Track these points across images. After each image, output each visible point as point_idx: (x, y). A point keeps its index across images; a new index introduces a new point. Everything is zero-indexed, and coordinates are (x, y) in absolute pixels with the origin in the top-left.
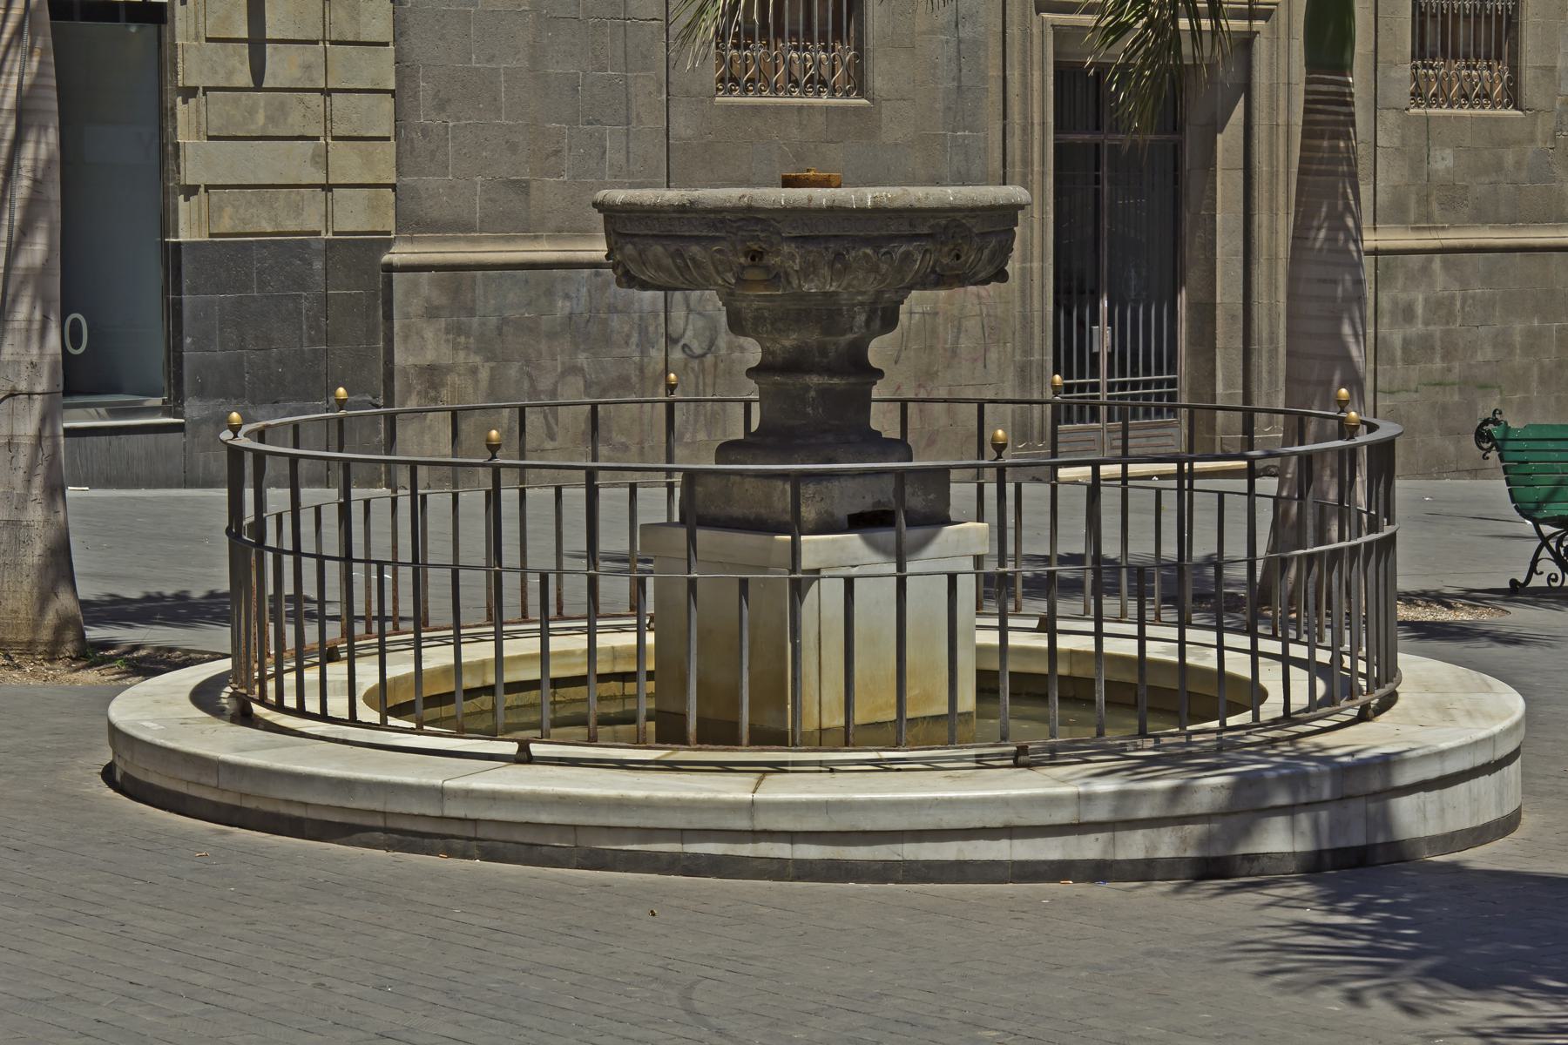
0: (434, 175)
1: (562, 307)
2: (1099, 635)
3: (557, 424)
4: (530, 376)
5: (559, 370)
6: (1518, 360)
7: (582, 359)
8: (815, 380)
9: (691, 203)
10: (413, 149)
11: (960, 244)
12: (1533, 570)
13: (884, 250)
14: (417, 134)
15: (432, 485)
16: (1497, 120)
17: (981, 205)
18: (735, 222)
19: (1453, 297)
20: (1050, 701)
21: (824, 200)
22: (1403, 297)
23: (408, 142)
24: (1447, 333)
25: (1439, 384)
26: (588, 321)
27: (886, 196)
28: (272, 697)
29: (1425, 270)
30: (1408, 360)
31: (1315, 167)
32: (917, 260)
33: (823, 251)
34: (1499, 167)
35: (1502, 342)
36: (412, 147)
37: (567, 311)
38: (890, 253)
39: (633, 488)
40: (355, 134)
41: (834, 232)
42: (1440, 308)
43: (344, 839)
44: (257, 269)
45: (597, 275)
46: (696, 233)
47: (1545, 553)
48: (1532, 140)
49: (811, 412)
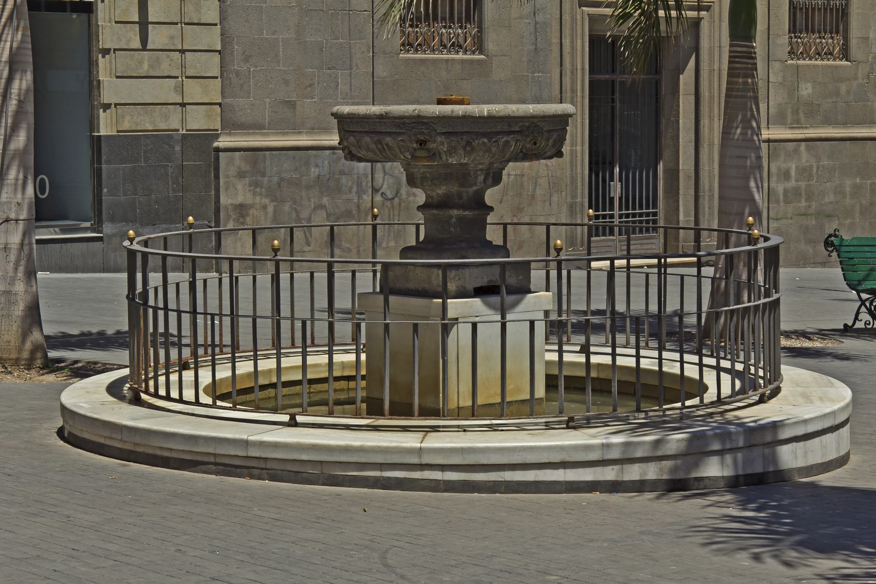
0: (242, 98)
2: (614, 355)
3: (311, 237)
4: (296, 210)
5: (312, 207)
6: (848, 201)
7: (325, 201)
8: (455, 212)
9: (386, 113)
10: (231, 83)
11: (537, 136)
12: (856, 318)
13: (494, 140)
14: (233, 75)
15: (241, 271)
16: (836, 67)
17: (548, 114)
18: (411, 124)
19: (812, 166)
20: (586, 392)
21: (461, 112)
22: (784, 166)
23: (228, 79)
24: (808, 186)
25: (804, 215)
27: (495, 109)
28: (152, 390)
29: (796, 151)
30: (787, 201)
31: (734, 93)
32: (512, 145)
34: (837, 93)
35: (839, 191)
36: (230, 82)
37: (317, 174)
38: (497, 142)
39: (354, 273)
40: (198, 75)
41: (466, 130)
42: (804, 172)
43: (192, 469)
44: (143, 150)
45: (333, 153)
46: (389, 130)
47: (863, 309)
48: (856, 78)
49: (453, 230)
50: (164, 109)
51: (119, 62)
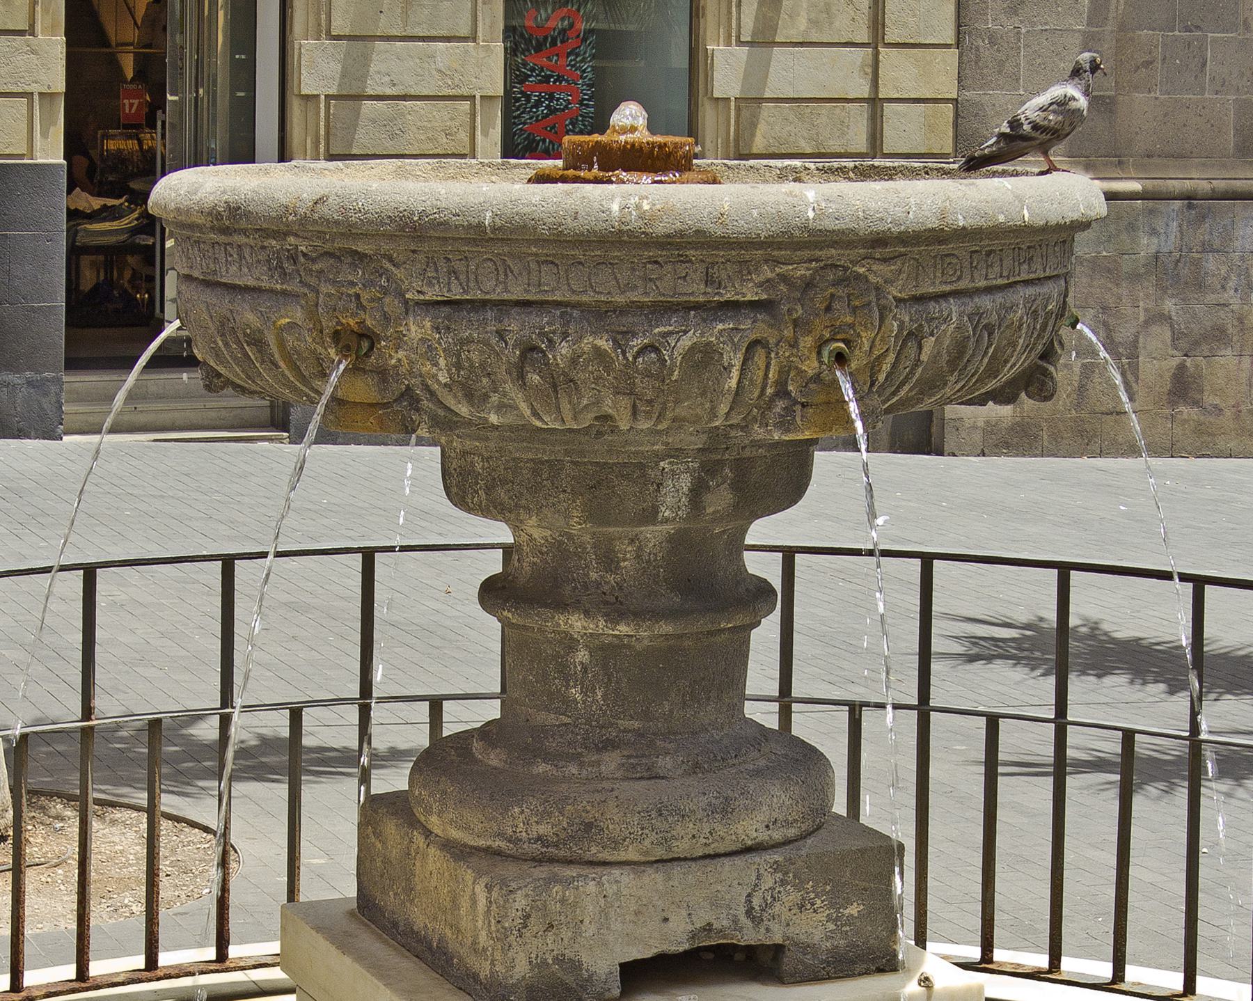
0: (1002, 89)
1: (1147, 245)
3: (1137, 382)
5: (1142, 318)
7: (1170, 305)
8: (577, 624)
11: (852, 326)
13: (636, 343)
14: (983, 41)
15: (986, 451)
17: (895, 230)
18: (314, 260)
21: (489, 214)
23: (973, 51)
26: (1178, 261)
27: (638, 207)
33: (494, 340)
36: (977, 56)
37: (1153, 249)
38: (656, 350)
40: (912, 41)
41: (517, 292)
45: (1190, 207)
49: (579, 697)
50: (838, 111)
51: (747, 12)
